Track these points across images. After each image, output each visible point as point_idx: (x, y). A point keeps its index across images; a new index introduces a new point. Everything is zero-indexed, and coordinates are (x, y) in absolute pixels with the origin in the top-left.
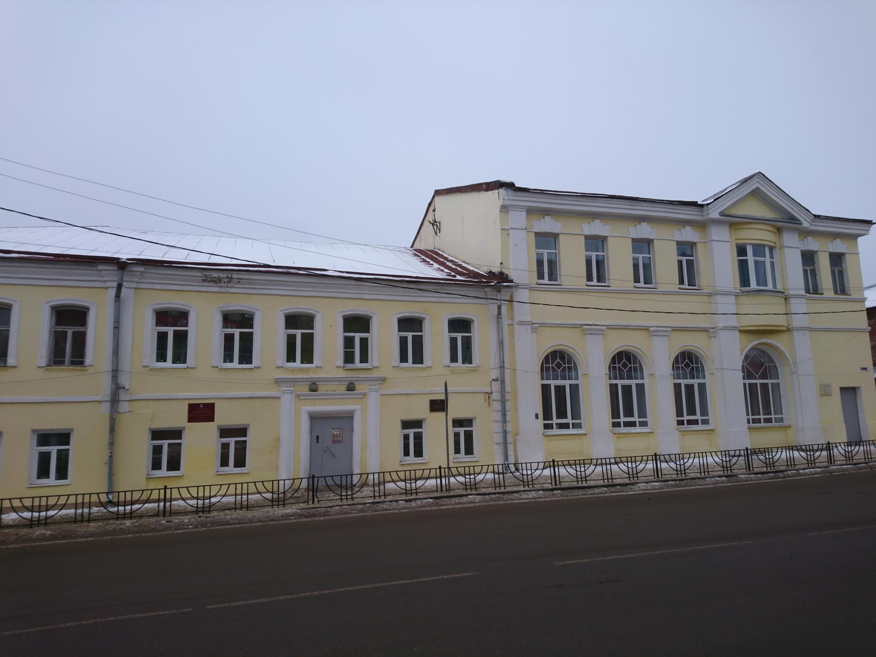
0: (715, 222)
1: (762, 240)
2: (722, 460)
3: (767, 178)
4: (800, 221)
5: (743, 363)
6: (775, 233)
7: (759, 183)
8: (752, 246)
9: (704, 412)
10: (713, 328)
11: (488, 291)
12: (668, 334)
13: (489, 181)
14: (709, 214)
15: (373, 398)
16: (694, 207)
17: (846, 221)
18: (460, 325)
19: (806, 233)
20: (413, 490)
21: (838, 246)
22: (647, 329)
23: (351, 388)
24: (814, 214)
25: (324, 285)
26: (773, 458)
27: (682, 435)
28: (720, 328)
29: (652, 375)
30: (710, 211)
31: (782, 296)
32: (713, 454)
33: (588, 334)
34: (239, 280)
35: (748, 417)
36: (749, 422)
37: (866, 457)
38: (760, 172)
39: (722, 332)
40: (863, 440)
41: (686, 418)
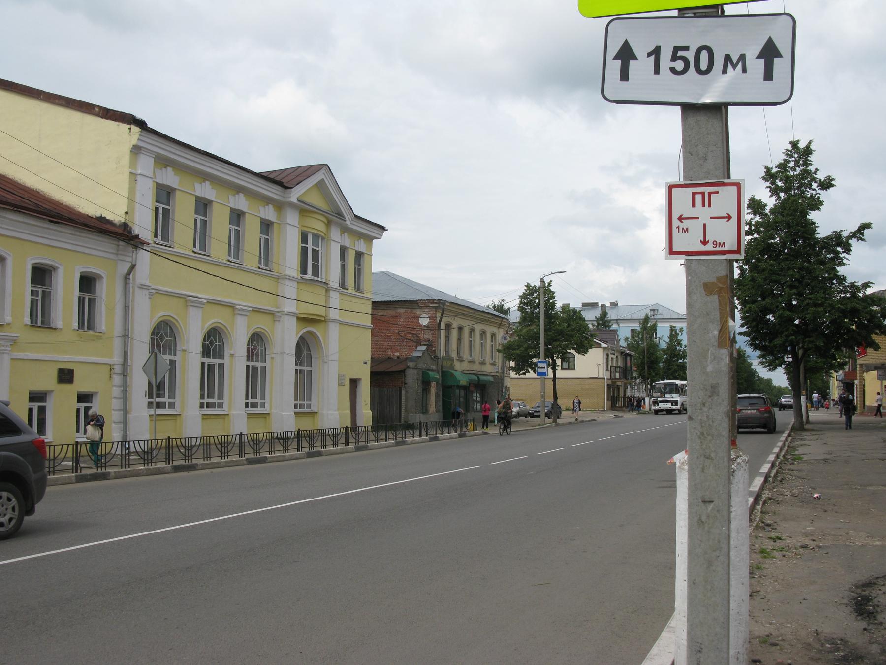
0: (292, 205)
3: (331, 172)
4: (345, 218)
5: (204, 340)
8: (313, 235)
9: (221, 396)
10: (278, 312)
12: (248, 314)
13: (109, 108)
16: (280, 187)
17: (205, 155)
18: (87, 282)
19: (345, 230)
21: (361, 246)
22: (233, 307)
24: (257, 172)
28: (285, 313)
29: (232, 355)
30: (292, 195)
31: (325, 286)
33: (239, 314)
35: (296, 402)
38: (327, 165)
39: (287, 317)
41: (206, 400)
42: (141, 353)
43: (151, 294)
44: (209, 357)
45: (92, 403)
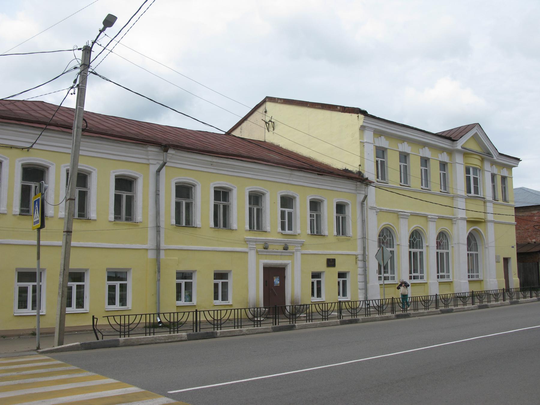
0: (458, 151)
1: (477, 165)
2: (214, 319)
5: (410, 238)
6: (480, 160)
7: (478, 130)
11: (358, 185)
12: (436, 220)
14: (457, 146)
15: (298, 255)
16: (450, 141)
18: (340, 208)
20: (172, 331)
21: (505, 173)
23: (286, 248)
25: (280, 174)
26: (221, 319)
27: (380, 287)
28: (459, 218)
29: (427, 246)
32: (206, 313)
33: (430, 221)
34: (212, 163)
35: (438, 274)
36: (469, 277)
37: (455, 304)
39: (460, 221)
40: (162, 311)
42: (373, 248)
43: (377, 212)
44: (413, 248)
45: (346, 278)
